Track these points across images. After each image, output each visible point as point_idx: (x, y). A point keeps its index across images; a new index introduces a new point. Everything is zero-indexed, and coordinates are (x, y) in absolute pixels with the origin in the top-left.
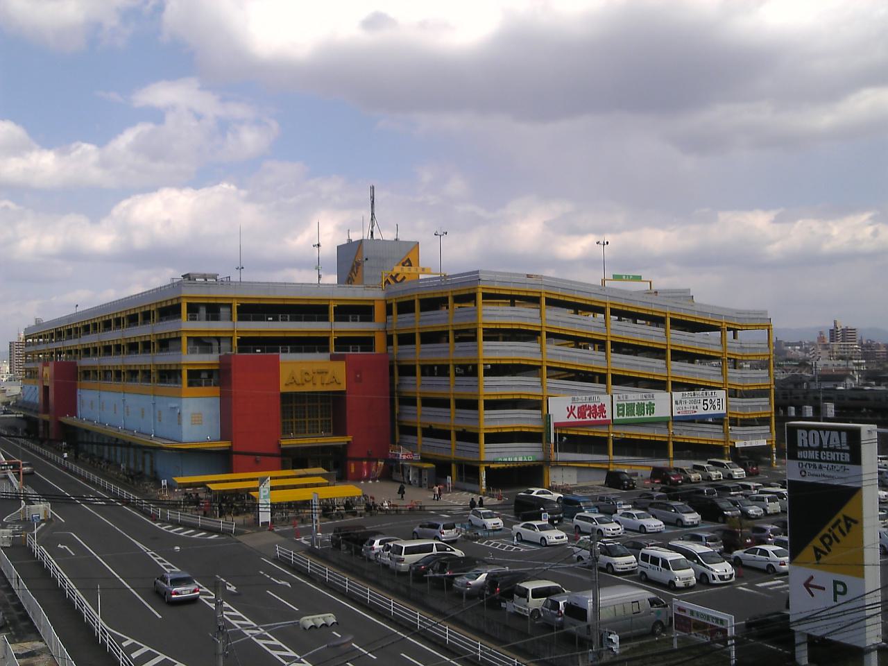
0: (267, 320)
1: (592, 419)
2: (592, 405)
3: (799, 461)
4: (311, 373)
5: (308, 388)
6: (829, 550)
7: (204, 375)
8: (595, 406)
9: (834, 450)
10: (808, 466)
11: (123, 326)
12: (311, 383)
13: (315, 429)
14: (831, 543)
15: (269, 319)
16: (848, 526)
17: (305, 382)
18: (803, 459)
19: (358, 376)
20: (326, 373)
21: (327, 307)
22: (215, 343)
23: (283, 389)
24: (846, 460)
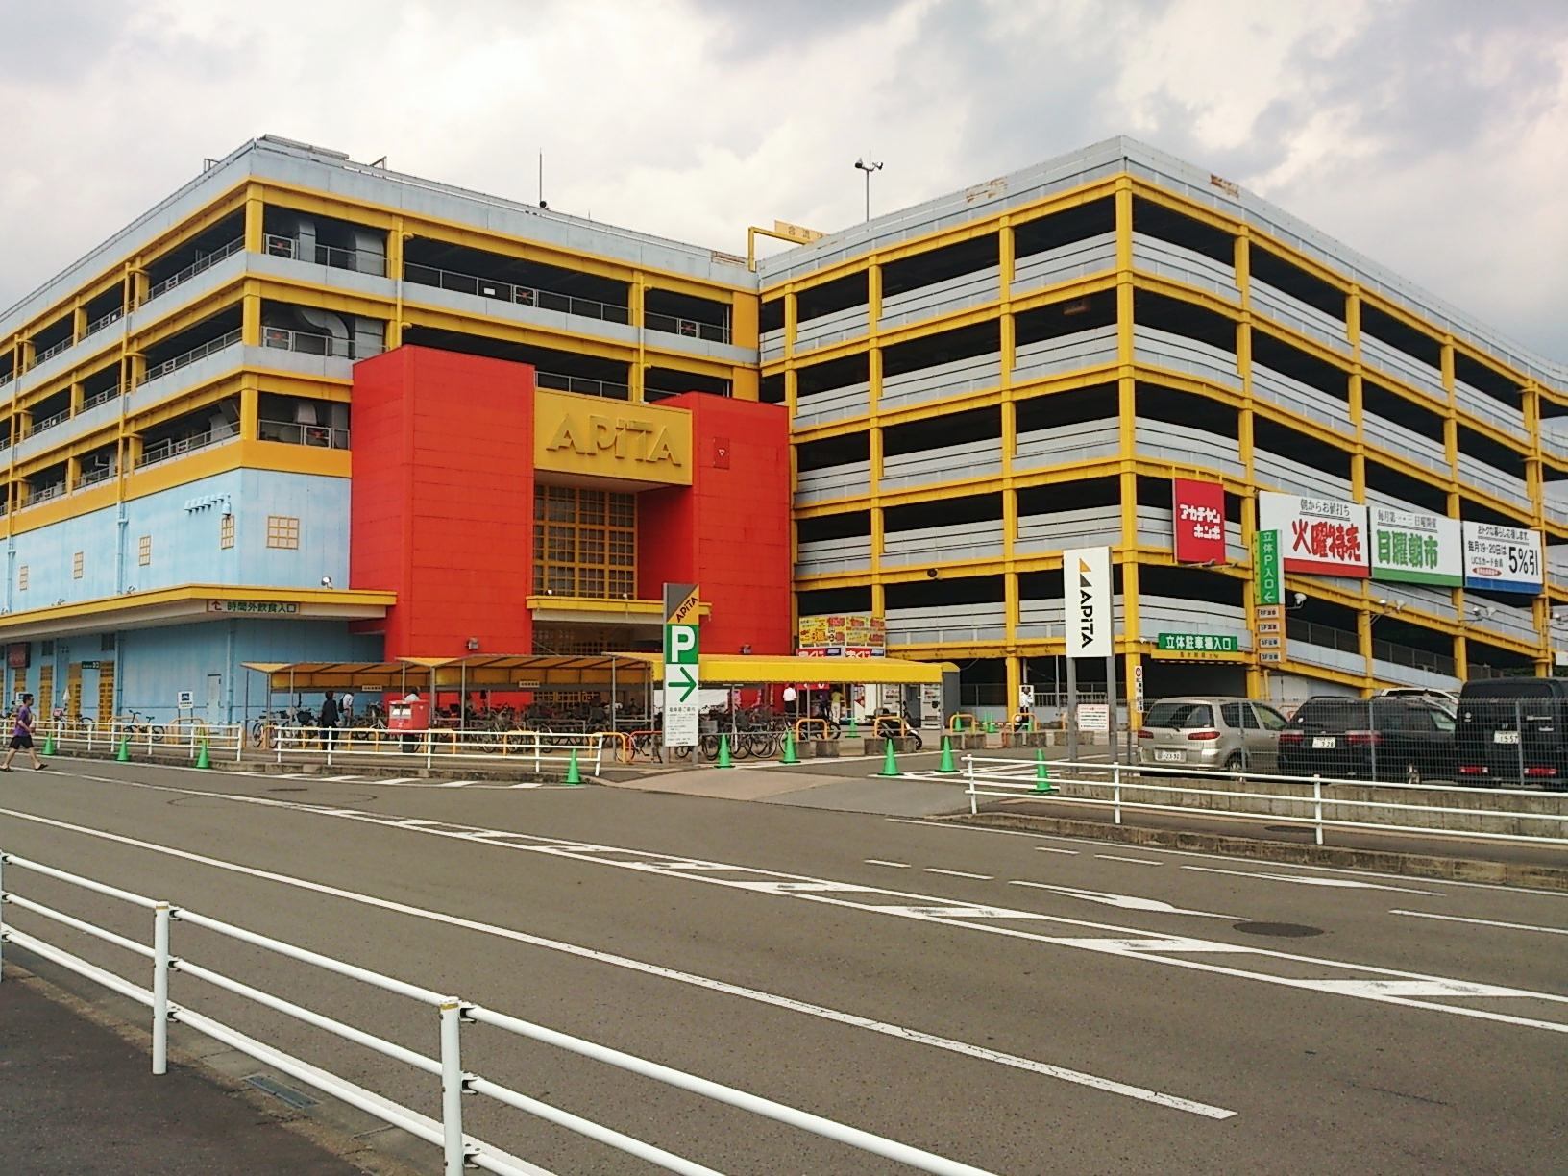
0: (482, 294)
1: (1338, 560)
2: (1336, 523)
4: (611, 427)
5: (604, 467)
6: (1082, 608)
7: (306, 416)
8: (1341, 528)
11: (14, 505)
12: (611, 454)
14: (1085, 612)
15: (487, 291)
16: (1085, 636)
17: (596, 450)
19: (722, 452)
20: (649, 433)
21: (625, 287)
22: (339, 331)
23: (543, 461)
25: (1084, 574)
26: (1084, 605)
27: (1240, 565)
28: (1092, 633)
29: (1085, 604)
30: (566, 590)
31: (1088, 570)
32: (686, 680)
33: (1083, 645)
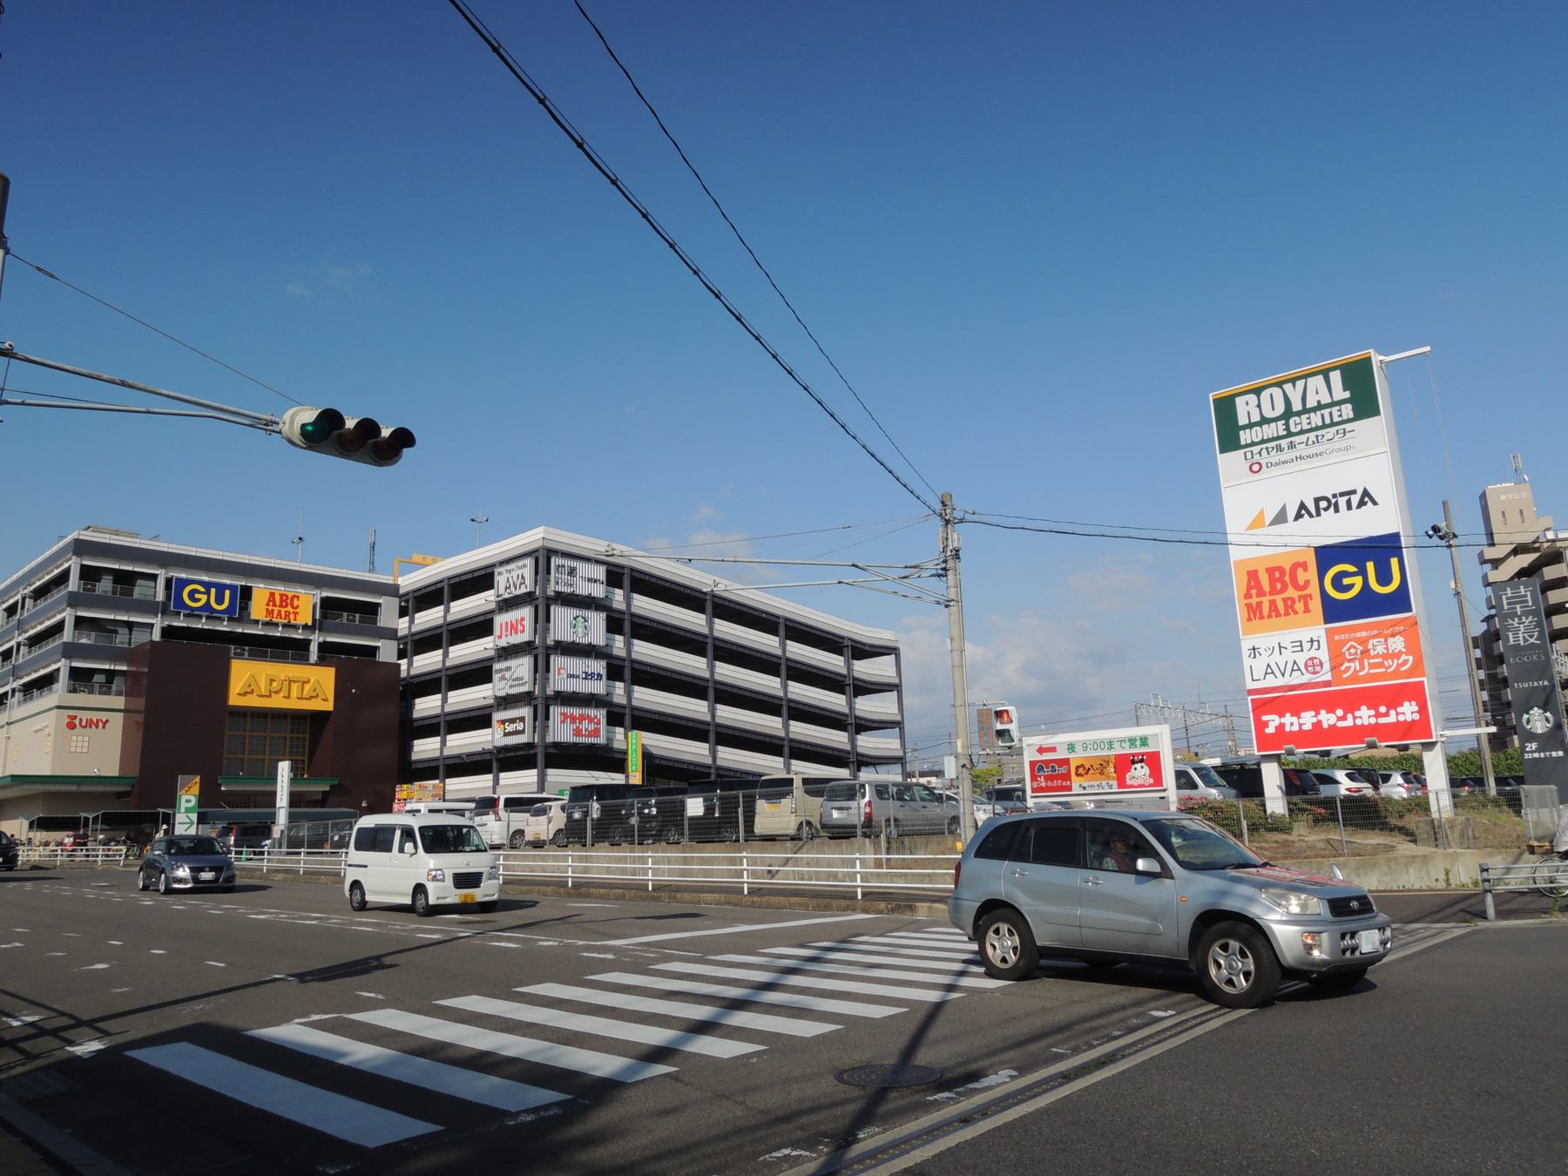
3: (1243, 451)
5: (277, 702)
6: (1318, 514)
9: (1320, 407)
10: (1264, 452)
13: (300, 750)
14: (1326, 509)
16: (1362, 504)
18: (1253, 444)
24: (1345, 417)
25: (1268, 519)
26: (1313, 511)
27: (1257, 403)
28: (1354, 492)
29: (1313, 510)
30: (301, 743)
31: (1261, 514)
32: (189, 821)
33: (1375, 503)
